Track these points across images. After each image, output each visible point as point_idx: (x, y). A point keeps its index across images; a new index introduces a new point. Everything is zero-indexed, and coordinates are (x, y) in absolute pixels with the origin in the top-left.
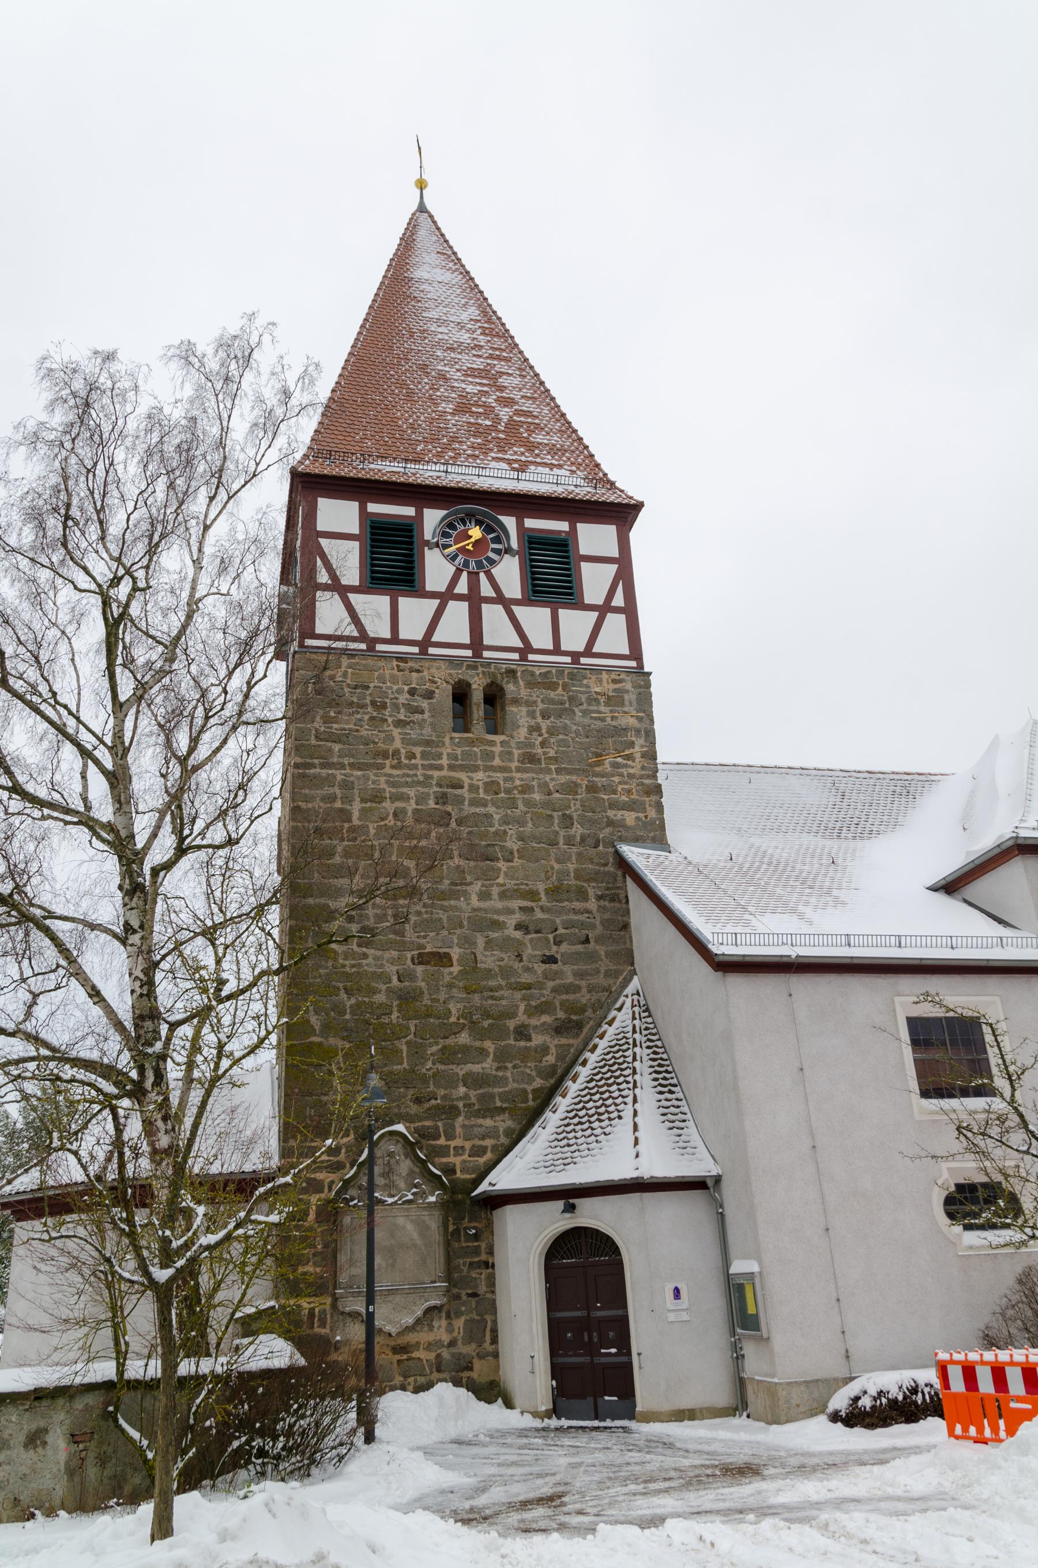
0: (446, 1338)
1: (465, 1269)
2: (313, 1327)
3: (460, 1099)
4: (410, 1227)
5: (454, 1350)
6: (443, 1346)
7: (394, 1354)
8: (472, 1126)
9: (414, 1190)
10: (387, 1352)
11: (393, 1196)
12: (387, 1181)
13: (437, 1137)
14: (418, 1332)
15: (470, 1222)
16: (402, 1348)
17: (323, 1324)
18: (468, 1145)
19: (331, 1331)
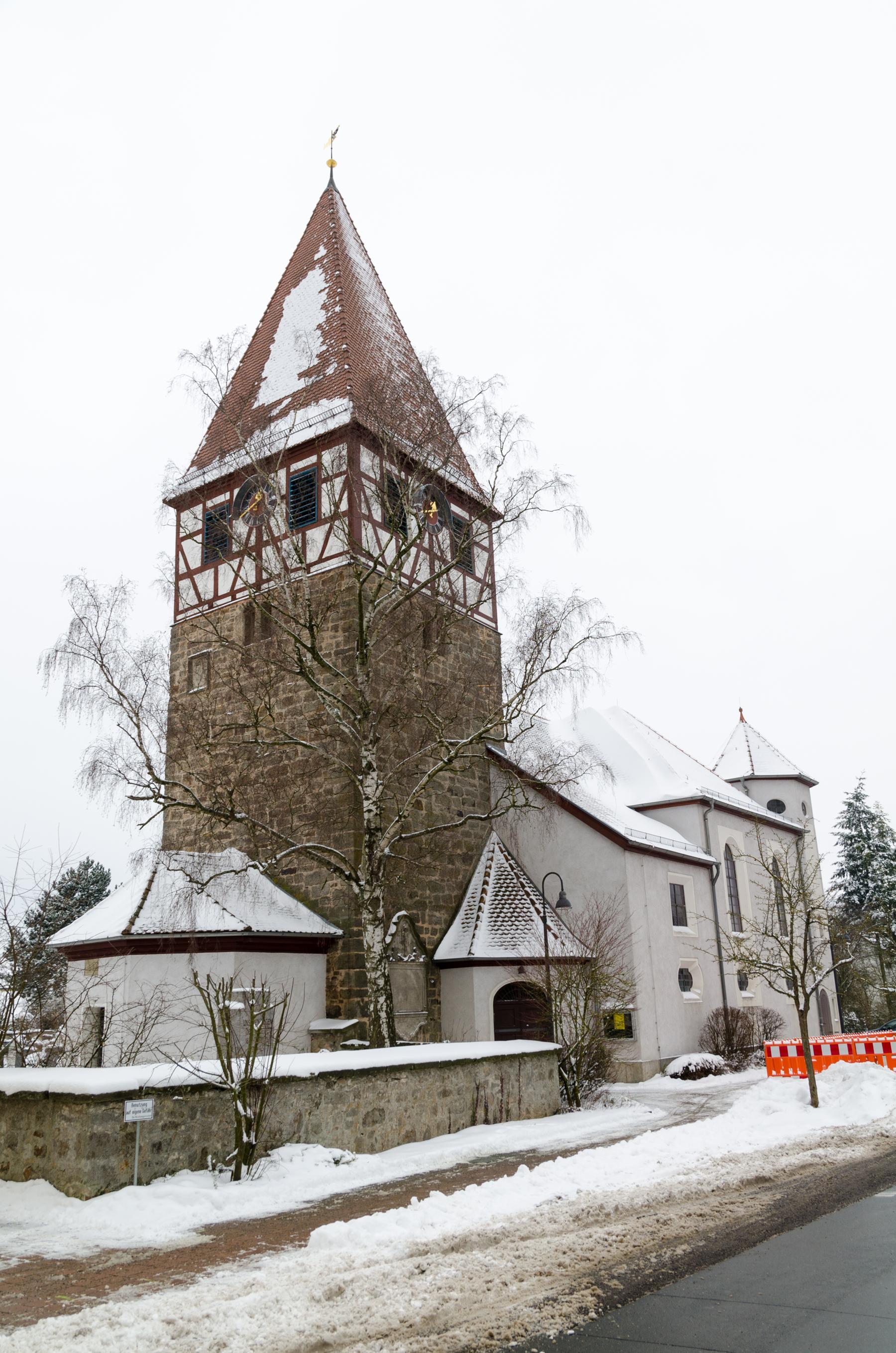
4: (412, 976)
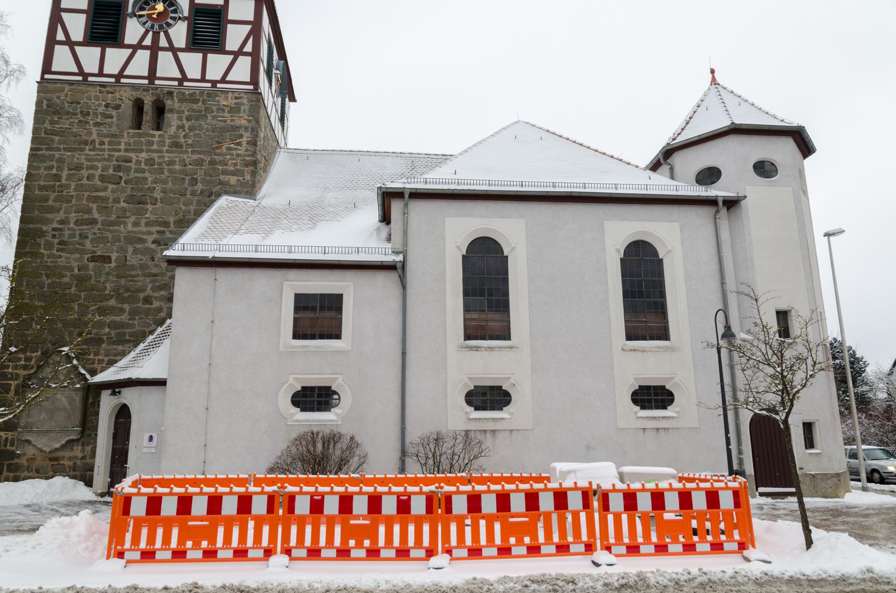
4: (64, 399)
18: (106, 359)
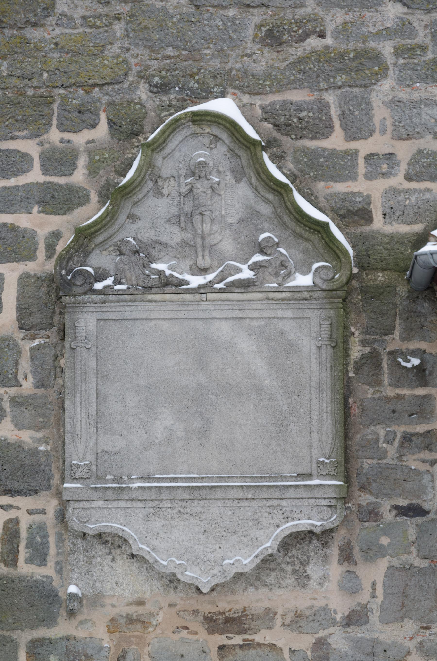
0: (340, 606)
1: (392, 450)
2: (14, 563)
3: (386, 33)
4: (246, 345)
5: (359, 633)
6: (334, 623)
7: (211, 631)
8: (416, 105)
9: (258, 258)
10: (193, 627)
11: (204, 271)
12: (188, 236)
13: (323, 130)
14: (270, 587)
15: (406, 338)
16: (228, 620)
17: (39, 556)
18: (405, 151)
19: (59, 571)
